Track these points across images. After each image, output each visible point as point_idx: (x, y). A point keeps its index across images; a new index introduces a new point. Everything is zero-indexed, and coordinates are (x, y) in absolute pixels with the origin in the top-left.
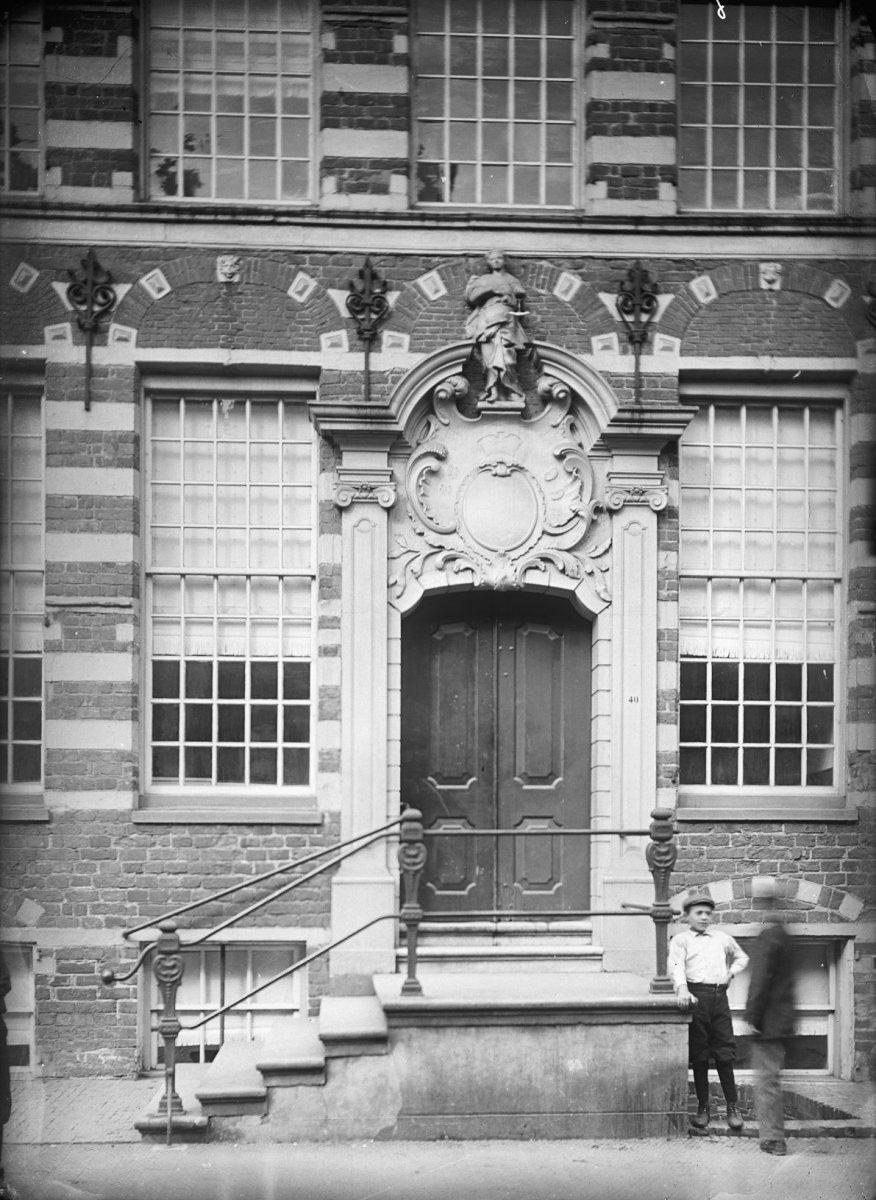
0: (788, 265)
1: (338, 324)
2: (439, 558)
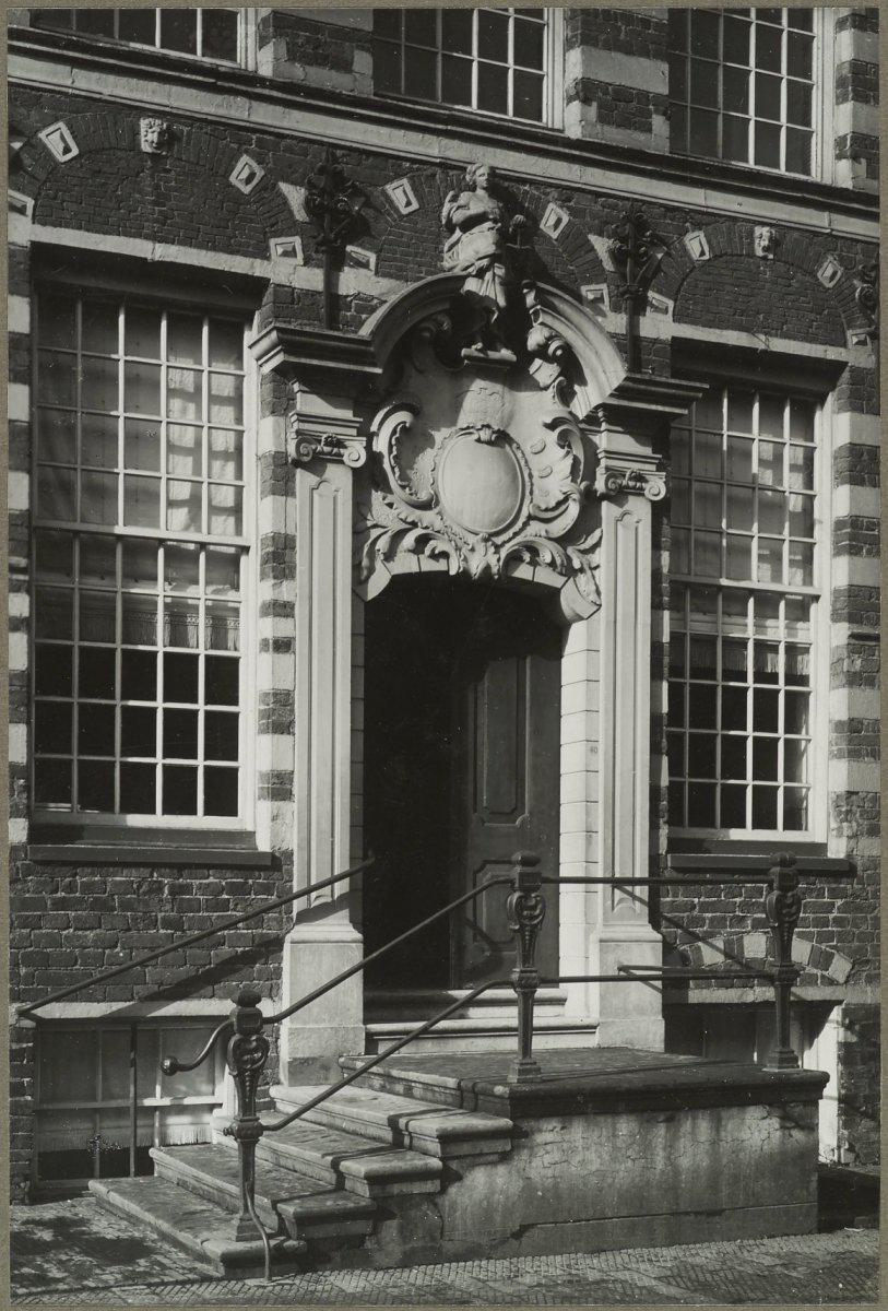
0: (781, 230)
1: (292, 227)
2: (409, 540)
